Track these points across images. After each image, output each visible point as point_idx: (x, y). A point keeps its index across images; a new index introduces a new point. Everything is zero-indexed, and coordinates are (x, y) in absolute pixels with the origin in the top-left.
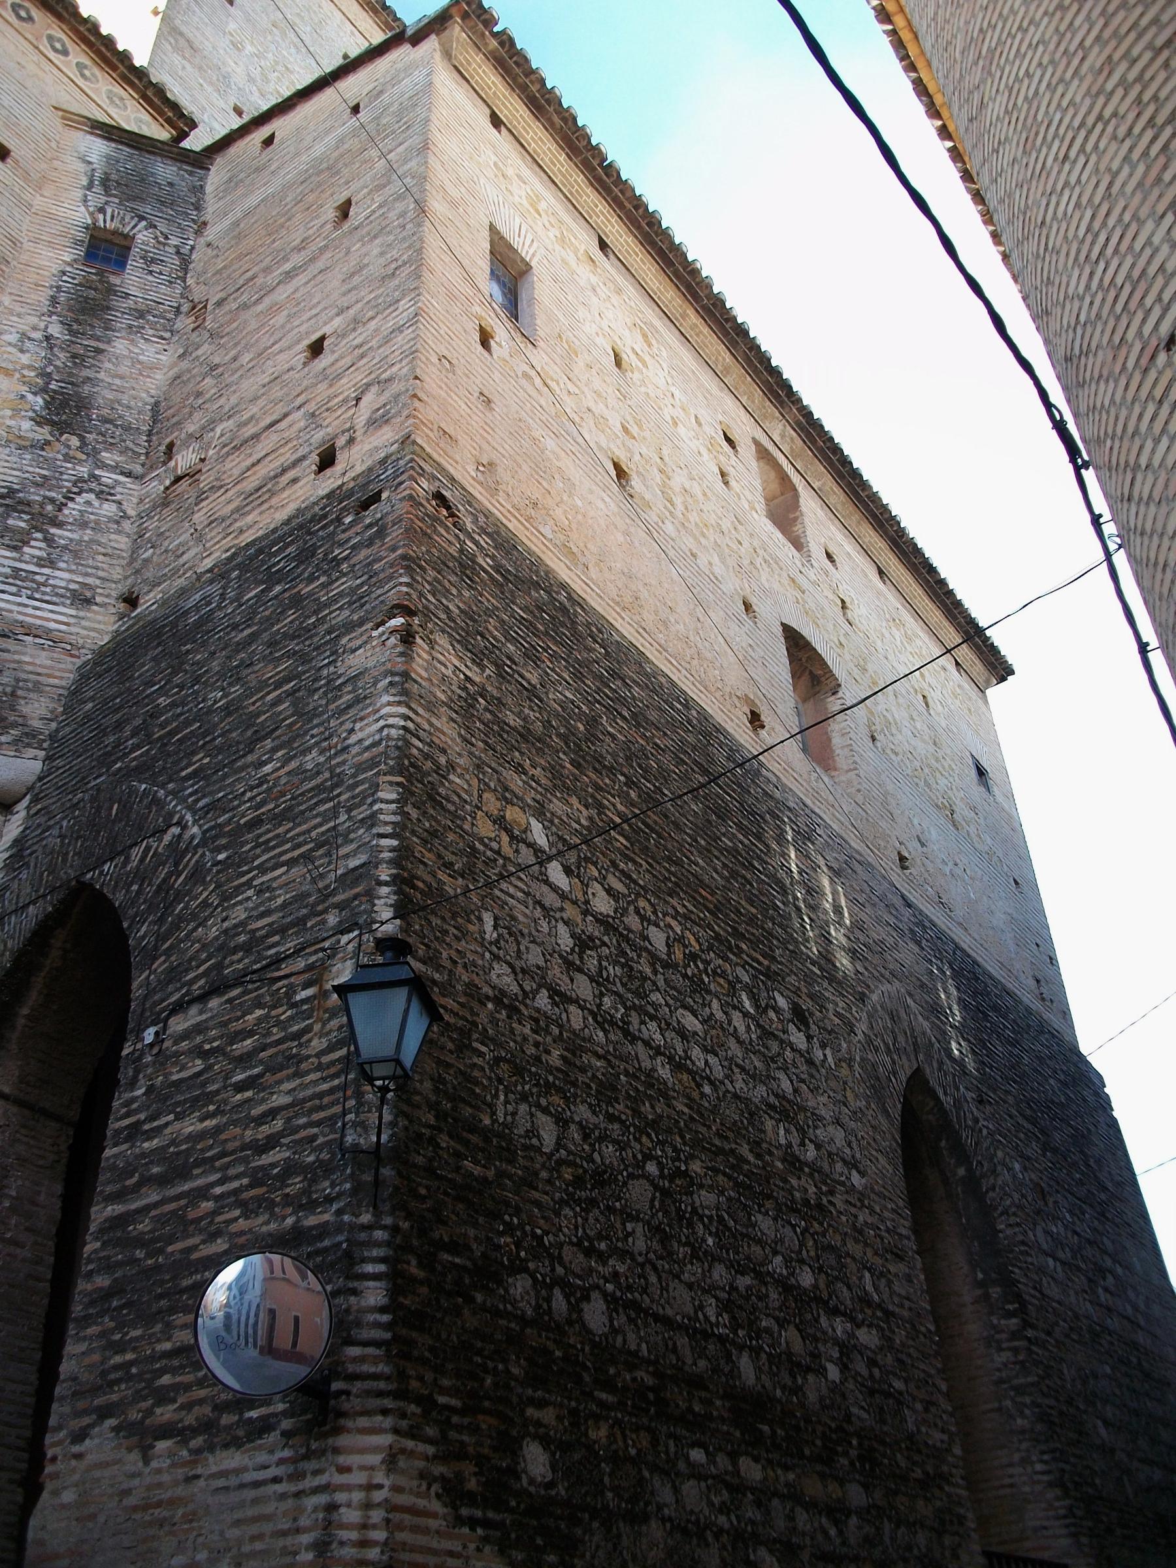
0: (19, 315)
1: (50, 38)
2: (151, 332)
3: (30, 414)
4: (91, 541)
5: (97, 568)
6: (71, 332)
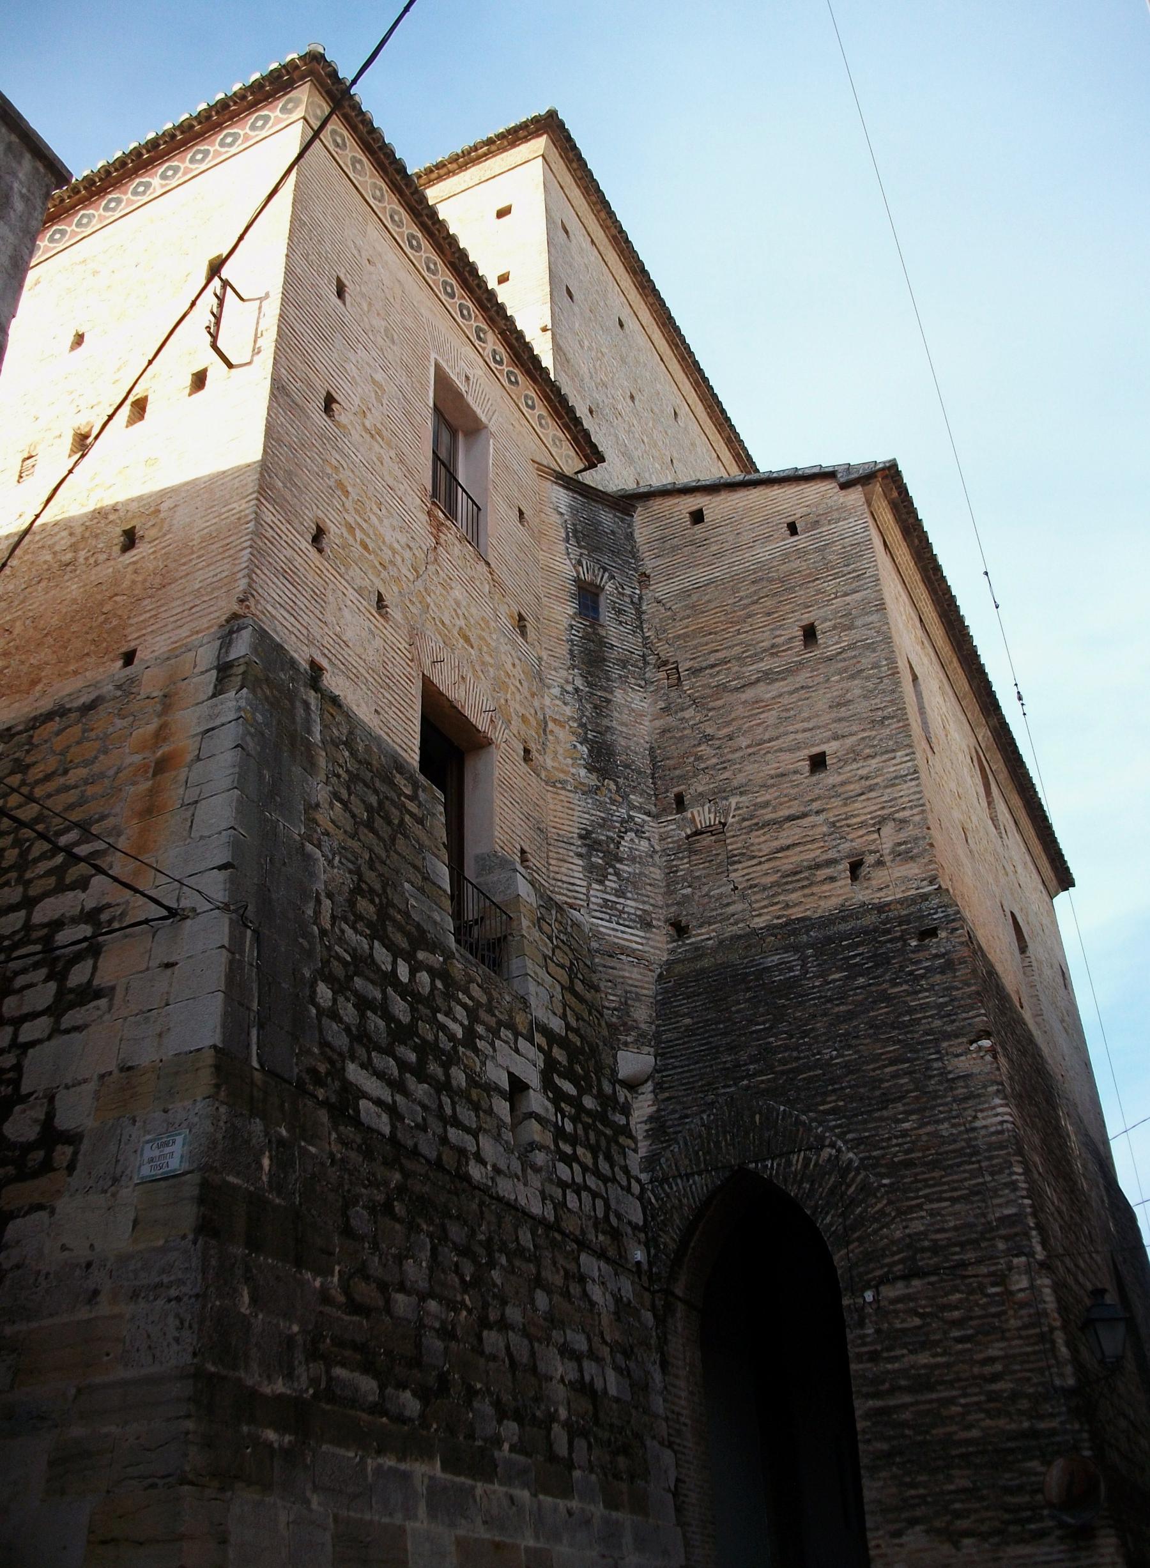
0: (555, 669)
1: (526, 397)
2: (633, 681)
3: (582, 762)
4: (641, 874)
5: (648, 896)
6: (590, 685)
